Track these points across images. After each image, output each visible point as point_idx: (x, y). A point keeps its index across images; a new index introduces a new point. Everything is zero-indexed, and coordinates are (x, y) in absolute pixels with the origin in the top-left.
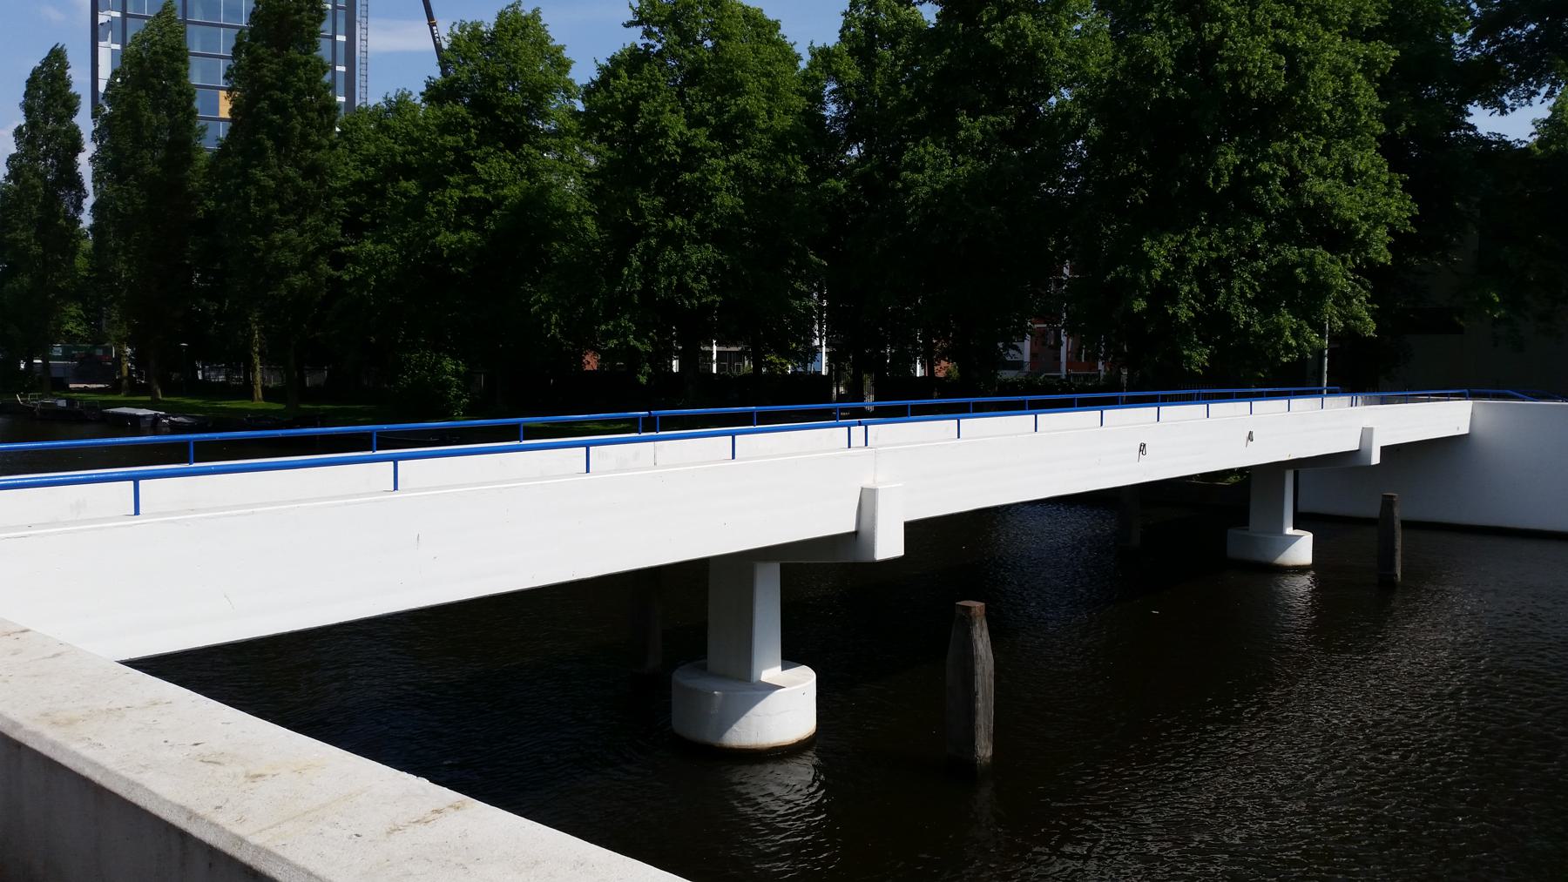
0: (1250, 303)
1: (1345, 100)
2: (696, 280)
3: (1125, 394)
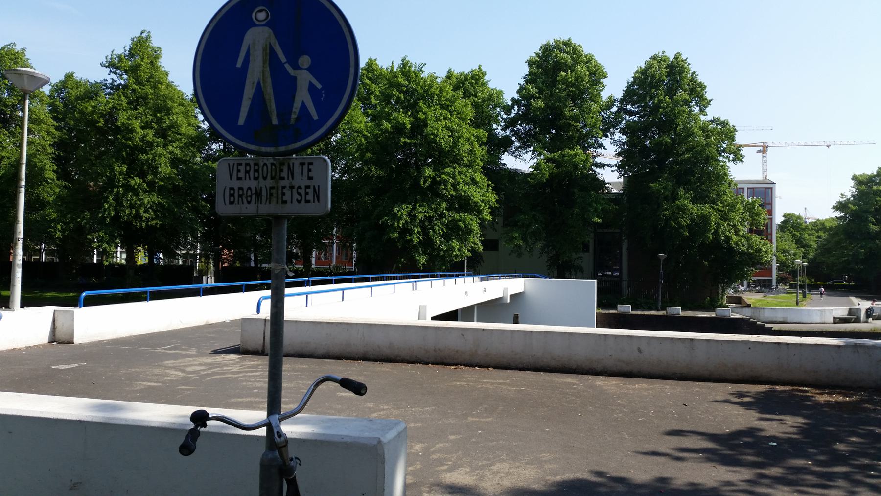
0: (442, 236)
1: (471, 152)
2: (146, 211)
3: (356, 277)
